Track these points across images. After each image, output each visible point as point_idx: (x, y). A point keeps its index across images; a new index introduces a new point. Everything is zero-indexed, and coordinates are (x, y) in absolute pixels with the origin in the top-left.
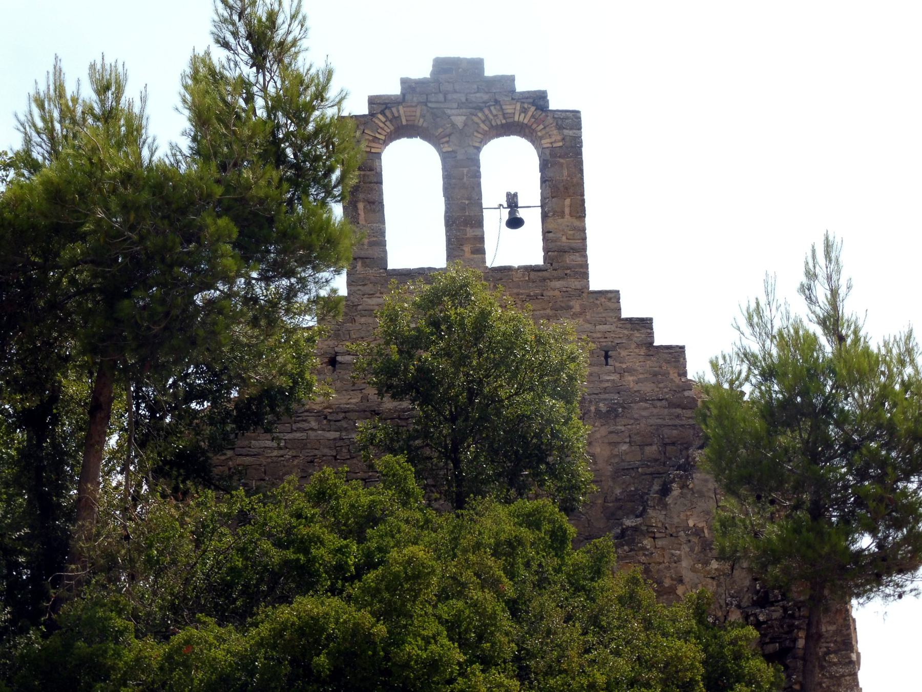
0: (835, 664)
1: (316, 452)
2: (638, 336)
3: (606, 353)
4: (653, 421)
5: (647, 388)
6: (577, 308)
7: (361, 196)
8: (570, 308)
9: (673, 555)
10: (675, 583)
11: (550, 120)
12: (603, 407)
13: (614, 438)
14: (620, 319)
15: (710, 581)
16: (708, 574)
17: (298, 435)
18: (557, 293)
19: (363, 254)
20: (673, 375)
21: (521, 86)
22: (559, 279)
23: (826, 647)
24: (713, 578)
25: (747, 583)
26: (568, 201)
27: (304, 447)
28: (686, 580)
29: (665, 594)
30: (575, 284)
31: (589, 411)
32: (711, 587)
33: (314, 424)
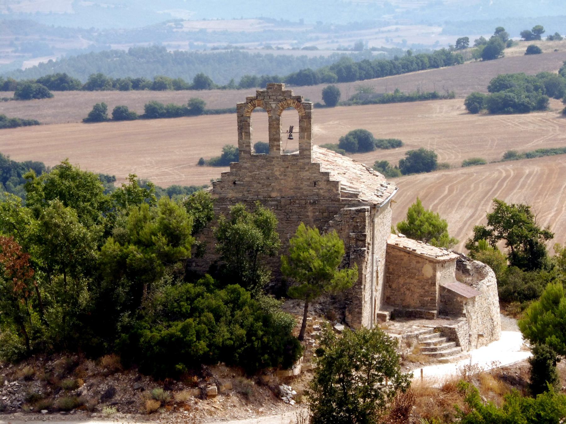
2: (325, 178)
4: (327, 205)
5: (326, 194)
6: (307, 168)
7: (243, 131)
11: (301, 106)
12: (312, 201)
13: (315, 210)
14: (319, 172)
17: (224, 206)
19: (243, 149)
20: (334, 190)
22: (302, 159)
25: (342, 260)
26: (306, 134)
27: (226, 210)
30: (306, 161)
33: (228, 203)
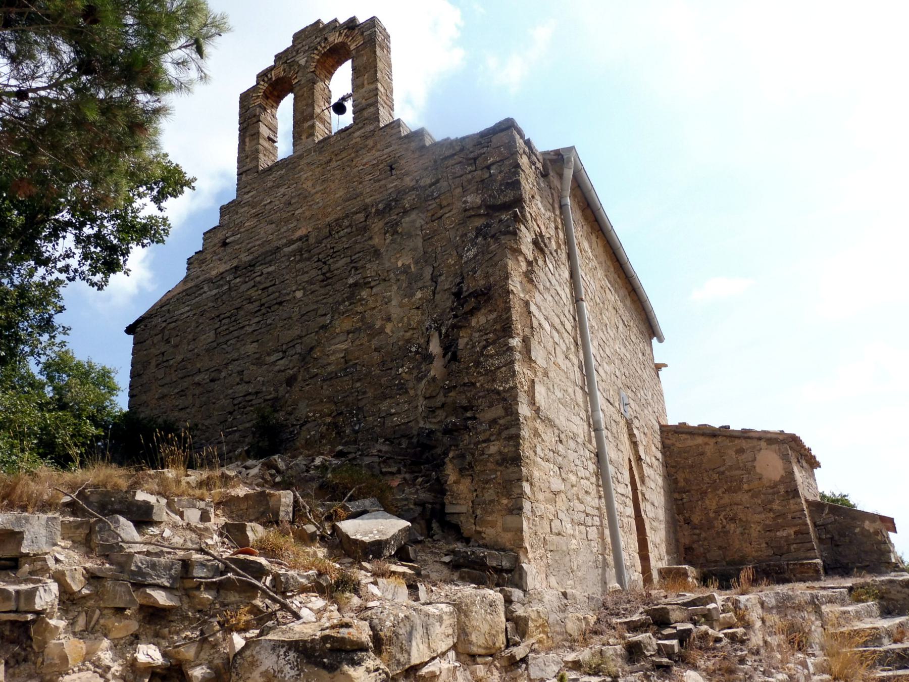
0: (492, 356)
1: (206, 307)
3: (391, 167)
8: (366, 146)
9: (384, 297)
10: (384, 322)
15: (416, 311)
16: (413, 305)
18: (358, 139)
21: (342, 20)
23: (485, 340)
24: (418, 308)
28: (394, 316)
29: (376, 335)
31: (370, 213)
32: (417, 316)
